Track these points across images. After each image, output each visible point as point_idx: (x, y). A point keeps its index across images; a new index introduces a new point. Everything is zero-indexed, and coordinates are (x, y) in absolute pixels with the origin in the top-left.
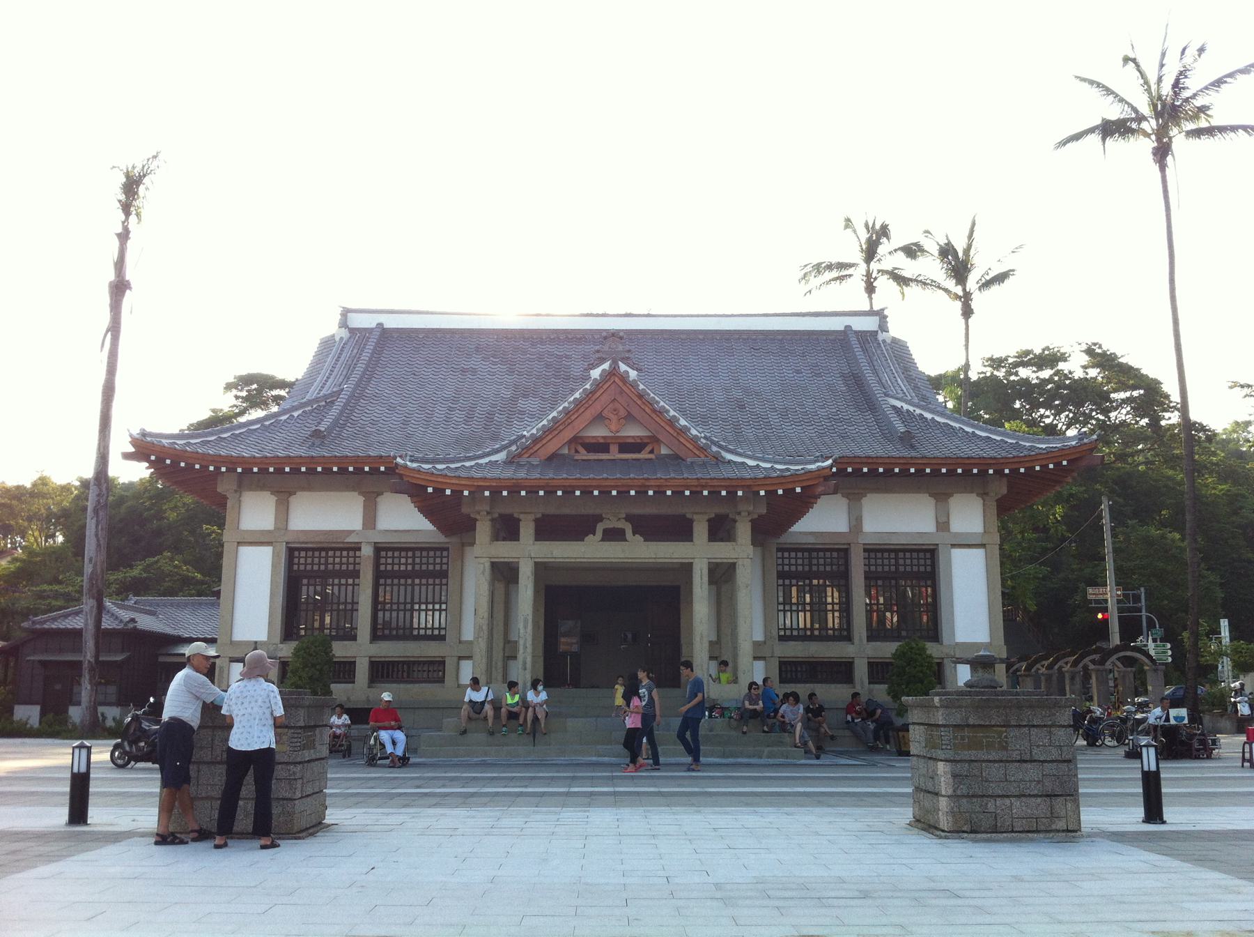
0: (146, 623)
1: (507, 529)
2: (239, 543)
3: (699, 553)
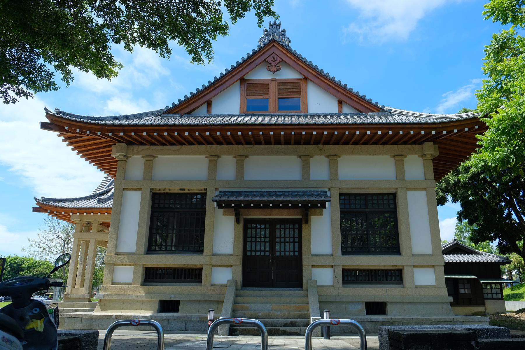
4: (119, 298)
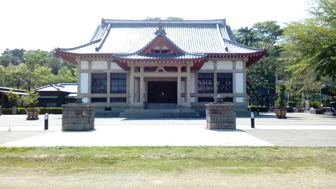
0: (62, 89)
1: (138, 69)
2: (81, 72)
3: (179, 75)
4: (220, 103)
